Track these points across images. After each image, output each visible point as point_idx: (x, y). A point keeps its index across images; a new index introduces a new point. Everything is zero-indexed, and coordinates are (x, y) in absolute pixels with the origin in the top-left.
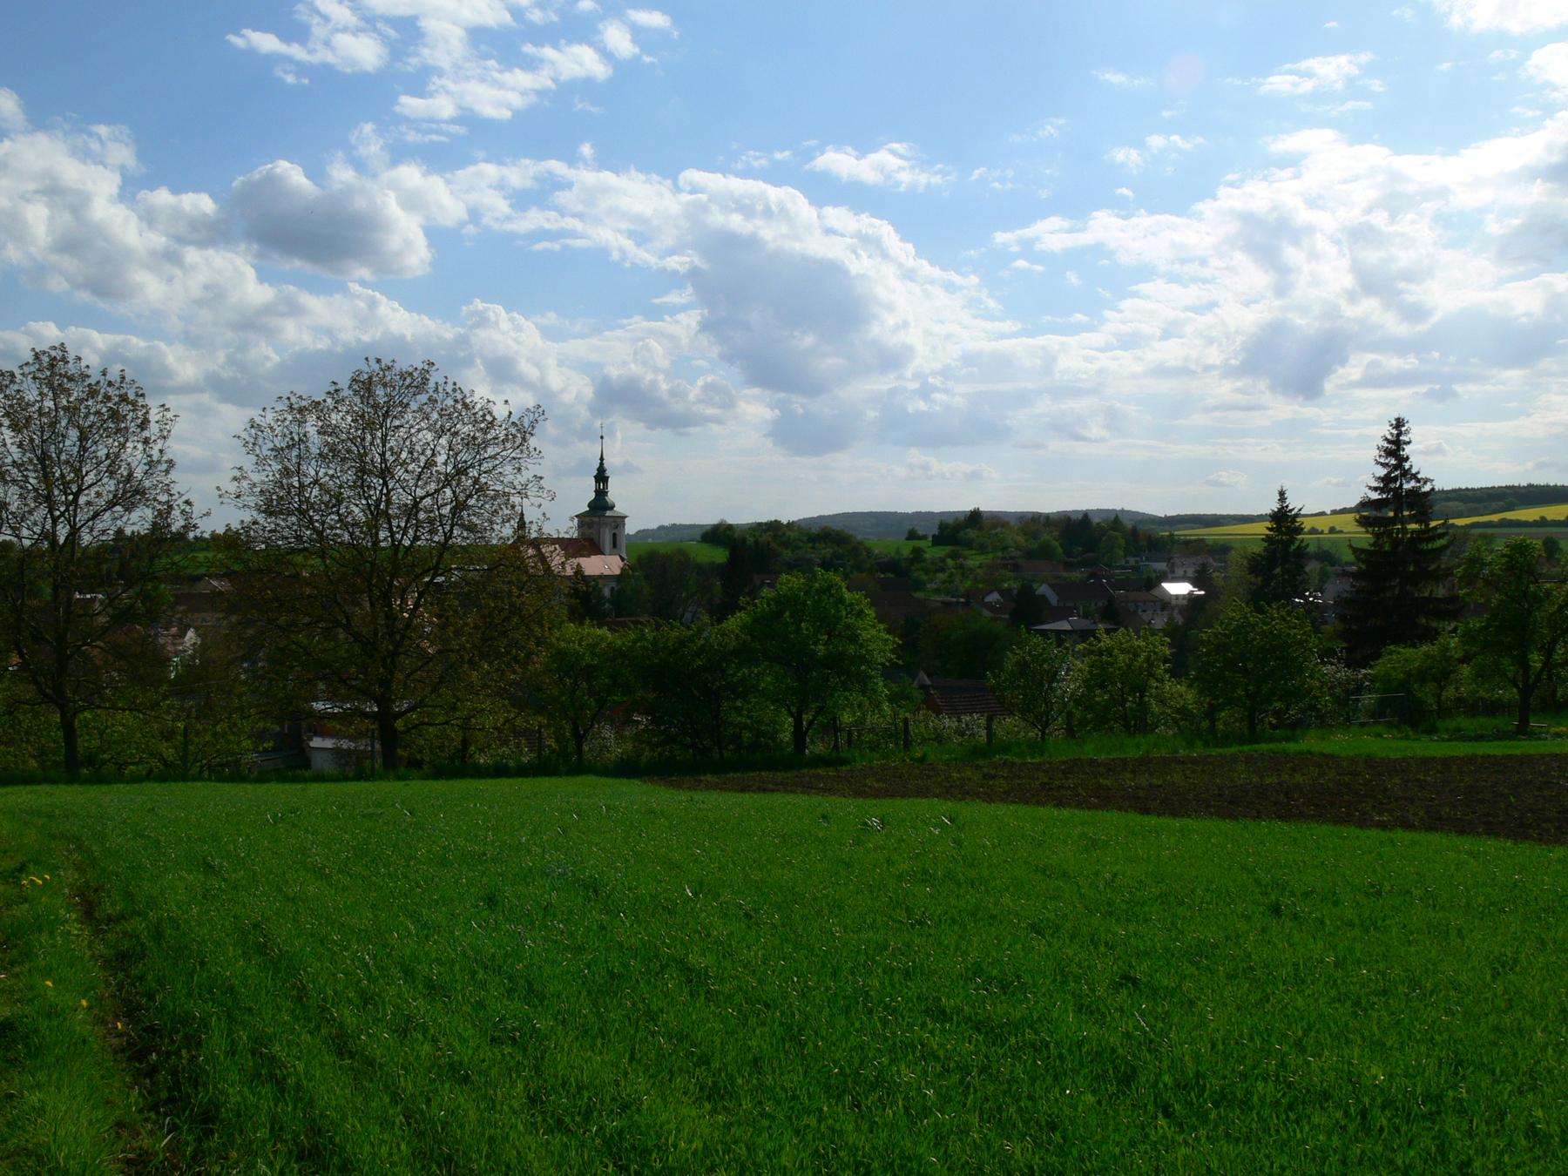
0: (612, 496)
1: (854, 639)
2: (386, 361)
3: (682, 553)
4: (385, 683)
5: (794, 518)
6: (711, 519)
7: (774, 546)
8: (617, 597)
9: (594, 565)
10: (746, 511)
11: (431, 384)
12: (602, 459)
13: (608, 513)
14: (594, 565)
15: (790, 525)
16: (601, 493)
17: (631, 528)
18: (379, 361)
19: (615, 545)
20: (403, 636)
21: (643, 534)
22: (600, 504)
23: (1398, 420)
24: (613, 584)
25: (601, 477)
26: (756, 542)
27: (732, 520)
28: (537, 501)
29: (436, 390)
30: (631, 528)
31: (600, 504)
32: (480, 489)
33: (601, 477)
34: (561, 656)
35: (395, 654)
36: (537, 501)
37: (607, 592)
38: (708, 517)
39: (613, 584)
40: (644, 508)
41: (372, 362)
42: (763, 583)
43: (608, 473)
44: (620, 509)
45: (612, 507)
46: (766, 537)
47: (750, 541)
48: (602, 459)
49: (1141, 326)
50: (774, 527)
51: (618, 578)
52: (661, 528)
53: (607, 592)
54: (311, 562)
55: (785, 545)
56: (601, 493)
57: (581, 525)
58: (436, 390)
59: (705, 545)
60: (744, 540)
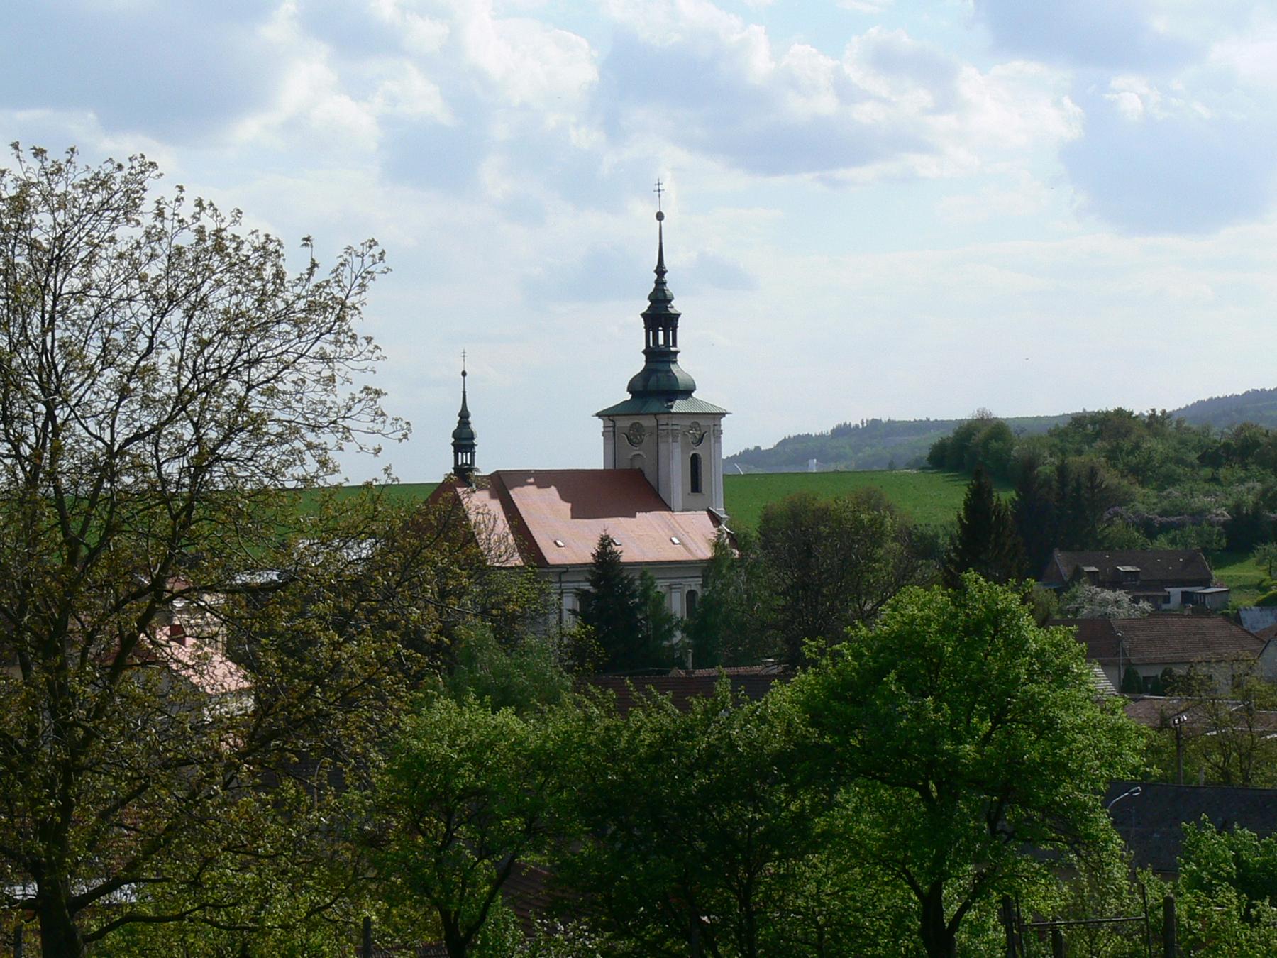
0: (686, 366)
1: (1047, 728)
2: (56, 154)
3: (870, 501)
4: (52, 833)
6: (955, 407)
7: (1110, 478)
8: (704, 615)
9: (645, 538)
10: (1036, 384)
11: (148, 206)
12: (660, 271)
13: (679, 406)
15: (1156, 423)
16: (660, 357)
17: (734, 440)
18: (39, 153)
19: (696, 487)
20: (90, 735)
22: (657, 385)
24: (695, 584)
25: (660, 316)
26: (1062, 470)
27: (1006, 408)
28: (372, 442)
29: (160, 214)
30: (734, 440)
31: (657, 385)
32: (245, 423)
33: (660, 316)
34: (415, 769)
35: (69, 770)
36: (372, 442)
37: (676, 605)
38: (952, 403)
39: (695, 584)
40: (775, 386)
41: (27, 154)
42: (1077, 574)
43: (676, 306)
44: (706, 396)
45: (687, 392)
46: (1093, 456)
47: (1047, 467)
48: (660, 271)
50: (1111, 428)
51: (708, 569)
52: (842, 431)
53: (676, 605)
54: (206, 354)
55: (1141, 473)
56: (660, 357)
57: (611, 434)
58: (160, 214)
59: (938, 478)
60: (1030, 464)
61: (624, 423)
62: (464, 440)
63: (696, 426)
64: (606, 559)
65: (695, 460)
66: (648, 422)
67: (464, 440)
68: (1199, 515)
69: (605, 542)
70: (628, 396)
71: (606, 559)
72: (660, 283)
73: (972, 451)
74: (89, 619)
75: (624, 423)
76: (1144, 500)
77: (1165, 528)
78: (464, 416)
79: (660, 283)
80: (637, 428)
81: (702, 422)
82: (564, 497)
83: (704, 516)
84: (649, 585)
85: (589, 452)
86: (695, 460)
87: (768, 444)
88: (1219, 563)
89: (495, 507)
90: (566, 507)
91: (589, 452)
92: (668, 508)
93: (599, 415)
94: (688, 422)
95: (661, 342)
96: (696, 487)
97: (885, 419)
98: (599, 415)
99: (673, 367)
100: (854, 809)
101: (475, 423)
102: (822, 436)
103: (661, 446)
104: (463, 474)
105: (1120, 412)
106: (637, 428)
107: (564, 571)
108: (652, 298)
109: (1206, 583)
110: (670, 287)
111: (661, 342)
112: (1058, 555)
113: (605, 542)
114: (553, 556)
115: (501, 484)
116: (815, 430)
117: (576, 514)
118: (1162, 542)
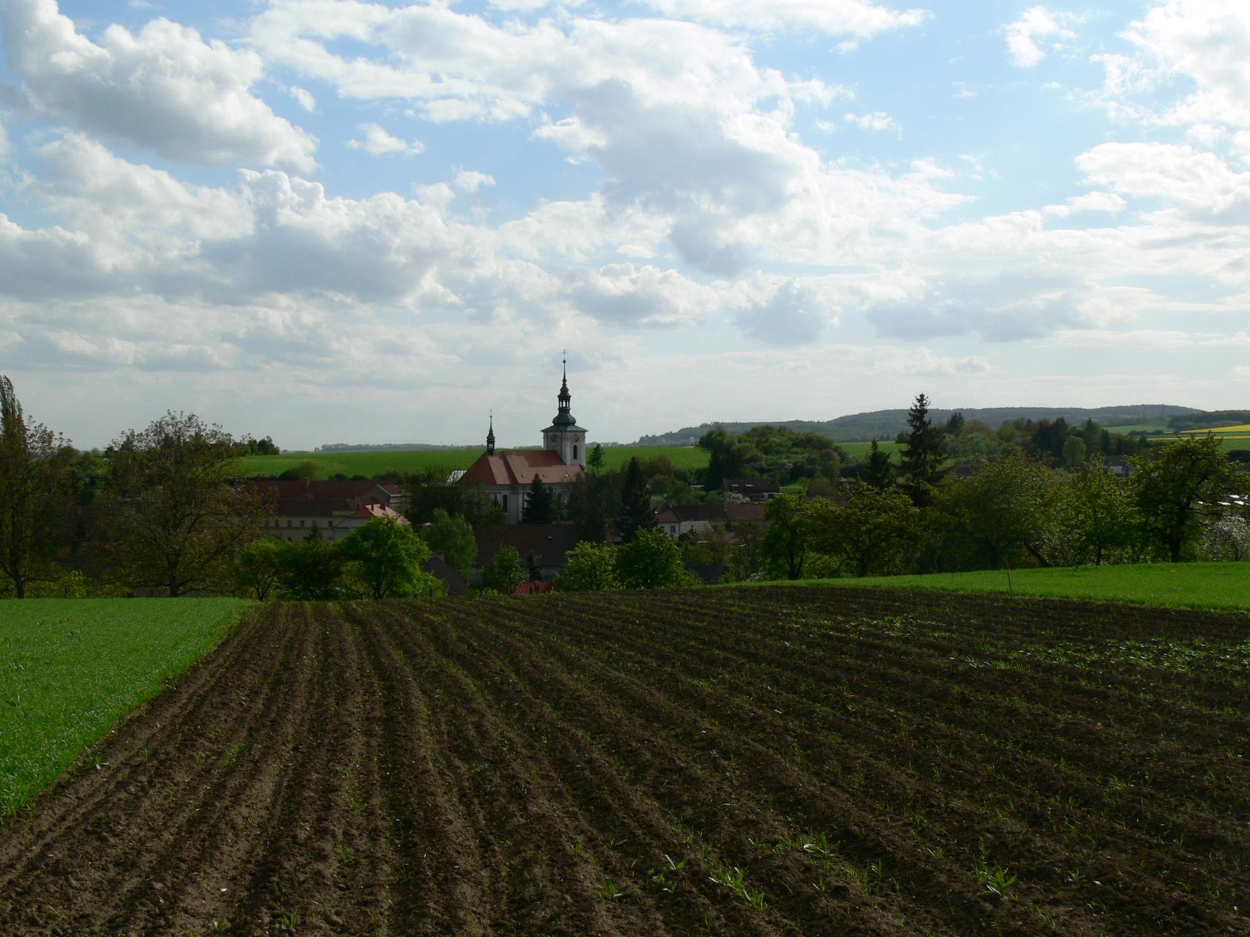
12: (564, 381)
13: (570, 428)
16: (564, 411)
17: (590, 439)
19: (575, 456)
22: (564, 421)
23: (922, 396)
30: (590, 439)
31: (564, 421)
33: (564, 396)
43: (570, 393)
48: (564, 381)
55: (766, 451)
56: (564, 411)
57: (546, 438)
59: (699, 449)
62: (491, 439)
64: (537, 482)
65: (575, 447)
66: (559, 434)
67: (491, 439)
68: (783, 465)
69: (537, 476)
71: (537, 482)
72: (564, 385)
73: (714, 440)
76: (765, 461)
77: (769, 470)
78: (491, 431)
79: (564, 385)
84: (551, 490)
85: (538, 441)
86: (575, 447)
87: (675, 431)
88: (782, 485)
89: (501, 462)
90: (527, 463)
91: (538, 441)
96: (575, 456)
100: (351, 565)
101: (495, 434)
104: (490, 451)
107: (524, 486)
109: (778, 491)
112: (725, 481)
113: (537, 476)
114: (521, 481)
115: (504, 454)
118: (765, 476)
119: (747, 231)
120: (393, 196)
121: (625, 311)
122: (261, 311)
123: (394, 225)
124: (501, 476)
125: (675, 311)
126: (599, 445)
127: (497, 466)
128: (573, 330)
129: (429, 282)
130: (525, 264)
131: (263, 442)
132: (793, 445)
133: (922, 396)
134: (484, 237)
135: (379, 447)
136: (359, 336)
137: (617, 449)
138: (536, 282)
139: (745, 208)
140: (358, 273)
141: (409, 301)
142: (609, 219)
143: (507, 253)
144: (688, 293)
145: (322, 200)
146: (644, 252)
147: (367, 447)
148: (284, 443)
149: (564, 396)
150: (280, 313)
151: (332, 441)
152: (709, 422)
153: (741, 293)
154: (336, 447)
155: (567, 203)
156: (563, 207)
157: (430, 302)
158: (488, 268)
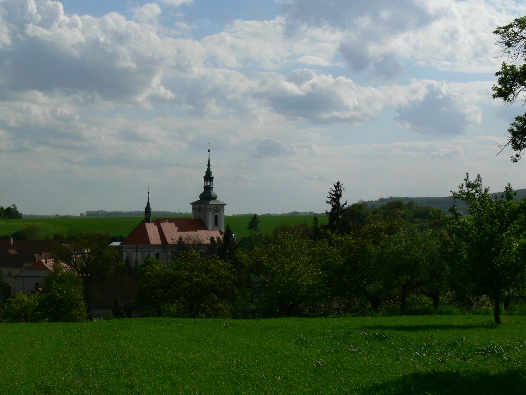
0: (215, 191)
5: (287, 213)
12: (209, 165)
13: (212, 202)
14: (204, 236)
16: (208, 189)
17: (228, 212)
19: (216, 223)
21: (230, 215)
22: (207, 195)
23: (338, 183)
27: (299, 211)
30: (228, 212)
31: (207, 195)
43: (213, 175)
44: (220, 199)
45: (215, 198)
48: (209, 165)
49: (387, 120)
56: (208, 189)
57: (194, 209)
61: (197, 206)
63: (217, 207)
65: (216, 217)
66: (203, 206)
70: (199, 199)
72: (209, 169)
74: (167, 385)
75: (197, 206)
78: (148, 204)
79: (209, 169)
80: (201, 208)
81: (218, 207)
82: (176, 225)
83: (218, 231)
85: (188, 210)
86: (216, 217)
89: (156, 228)
91: (188, 210)
92: (207, 229)
93: (191, 204)
94: (214, 206)
95: (208, 184)
96: (216, 223)
97: (394, 197)
98: (191, 204)
99: (211, 191)
102: (376, 201)
103: (207, 214)
105: (268, 214)
106: (201, 208)
108: (206, 172)
110: (212, 170)
111: (208, 184)
114: (169, 241)
116: (373, 200)
117: (179, 230)
119: (400, 44)
120: (115, 14)
121: (310, 107)
122: (24, 105)
123: (120, 38)
124: (154, 238)
125: (347, 109)
126: (256, 215)
127: (151, 230)
128: (265, 122)
129: (156, 84)
130: (228, 71)
131: (9, 209)
132: (415, 217)
133: (338, 183)
134: (195, 49)
135: (130, 213)
136: (104, 126)
137: (268, 218)
138: (242, 84)
139: (398, 26)
140: (93, 77)
141: (141, 98)
142: (290, 32)
143: (212, 61)
144: (352, 94)
145: (63, 17)
146: (323, 62)
147: (121, 213)
148: (24, 210)
149: (208, 177)
150: (40, 106)
151: (94, 208)
152: (385, 197)
153: (400, 94)
154: (97, 213)
155: (254, 22)
156: (253, 25)
157: (156, 100)
158: (198, 71)
